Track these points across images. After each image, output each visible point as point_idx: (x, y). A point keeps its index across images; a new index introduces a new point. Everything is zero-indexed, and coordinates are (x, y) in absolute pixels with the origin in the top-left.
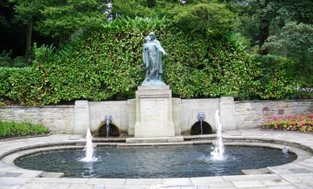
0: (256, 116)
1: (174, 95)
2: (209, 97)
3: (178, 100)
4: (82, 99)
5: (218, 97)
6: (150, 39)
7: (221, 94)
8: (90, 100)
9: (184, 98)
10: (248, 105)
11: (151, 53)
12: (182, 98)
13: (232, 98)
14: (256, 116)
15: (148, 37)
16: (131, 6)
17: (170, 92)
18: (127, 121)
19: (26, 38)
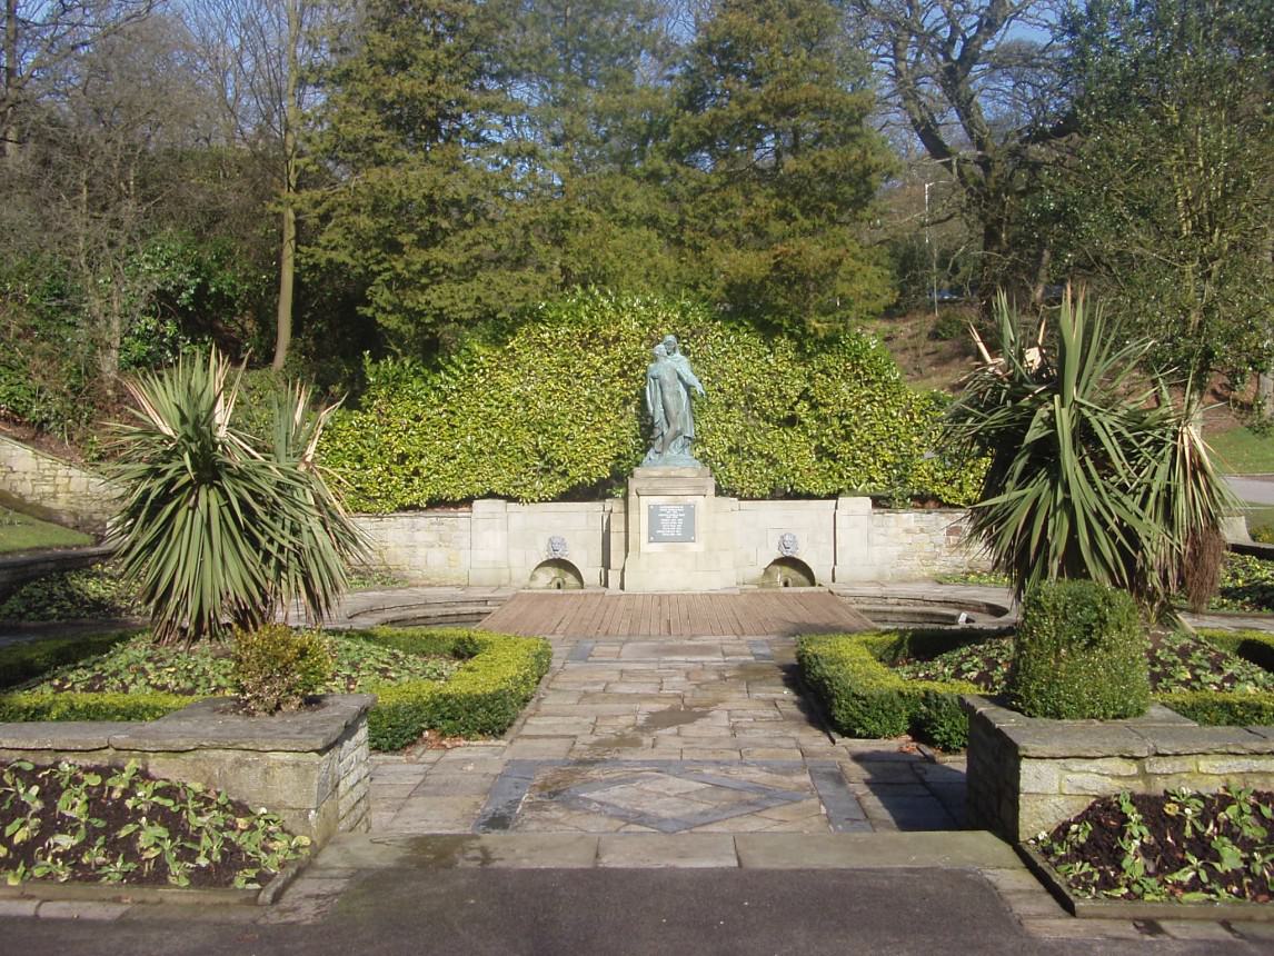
0: (929, 548)
1: (719, 492)
2: (810, 496)
3: (731, 503)
4: (492, 495)
5: (833, 496)
6: (664, 351)
7: (840, 491)
8: (509, 499)
9: (745, 499)
10: (909, 519)
11: (666, 389)
12: (741, 498)
13: (869, 501)
14: (929, 548)
15: (661, 346)
16: (873, 425)
17: (712, 482)
18: (321, 869)
19: (292, 347)
